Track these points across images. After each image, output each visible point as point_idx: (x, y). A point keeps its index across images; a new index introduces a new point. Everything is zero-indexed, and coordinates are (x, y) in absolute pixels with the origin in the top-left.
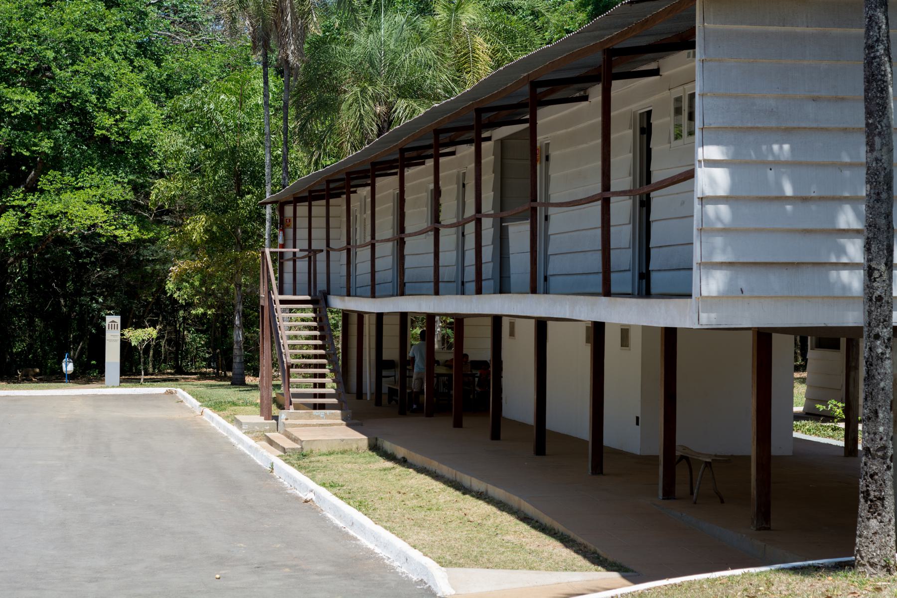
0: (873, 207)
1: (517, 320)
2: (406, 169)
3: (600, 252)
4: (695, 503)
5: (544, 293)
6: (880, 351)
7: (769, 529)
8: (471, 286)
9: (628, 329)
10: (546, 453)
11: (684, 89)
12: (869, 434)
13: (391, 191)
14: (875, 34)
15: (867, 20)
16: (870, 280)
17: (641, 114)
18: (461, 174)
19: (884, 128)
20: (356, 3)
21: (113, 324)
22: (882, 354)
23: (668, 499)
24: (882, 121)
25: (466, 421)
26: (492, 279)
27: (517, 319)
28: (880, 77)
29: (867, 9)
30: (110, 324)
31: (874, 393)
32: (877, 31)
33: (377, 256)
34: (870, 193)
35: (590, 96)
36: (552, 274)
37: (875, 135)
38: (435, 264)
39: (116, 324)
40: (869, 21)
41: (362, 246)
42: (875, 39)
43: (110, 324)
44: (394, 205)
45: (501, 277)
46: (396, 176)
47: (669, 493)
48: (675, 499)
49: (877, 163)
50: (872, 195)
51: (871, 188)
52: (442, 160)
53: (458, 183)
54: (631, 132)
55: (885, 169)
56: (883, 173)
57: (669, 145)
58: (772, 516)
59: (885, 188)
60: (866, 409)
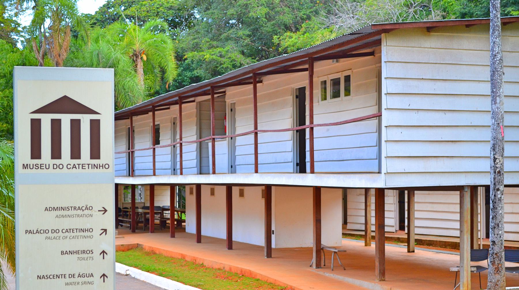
0: (496, 130)
1: (216, 187)
2: (133, 117)
3: (254, 155)
4: (333, 270)
5: (231, 173)
6: (499, 196)
7: (384, 280)
8: (179, 171)
9: (243, 189)
10: (233, 248)
11: (328, 77)
12: (494, 235)
13: (125, 126)
14: (496, 50)
15: (492, 43)
16: (495, 164)
17: (296, 89)
18: (173, 118)
19: (501, 93)
20: (302, 1)
21: (66, 119)
22: (500, 197)
23: (318, 268)
24: (500, 90)
25: (176, 235)
26: (196, 167)
27: (216, 186)
28: (499, 69)
29: (492, 38)
30: (46, 119)
31: (497, 216)
32: (498, 48)
33: (183, 152)
34: (494, 123)
35: (263, 81)
36: (238, 164)
37: (497, 96)
38: (180, 160)
39: (85, 120)
40: (493, 44)
41: (308, 139)
42: (496, 52)
43: (46, 119)
44: (126, 133)
45: (200, 166)
46: (128, 120)
47: (318, 266)
48: (321, 268)
49: (498, 109)
50: (496, 124)
51: (495, 121)
52: (156, 112)
53: (171, 122)
54: (292, 97)
55: (501, 112)
56: (500, 114)
57: (318, 103)
58: (386, 274)
59: (501, 121)
60: (493, 223)
